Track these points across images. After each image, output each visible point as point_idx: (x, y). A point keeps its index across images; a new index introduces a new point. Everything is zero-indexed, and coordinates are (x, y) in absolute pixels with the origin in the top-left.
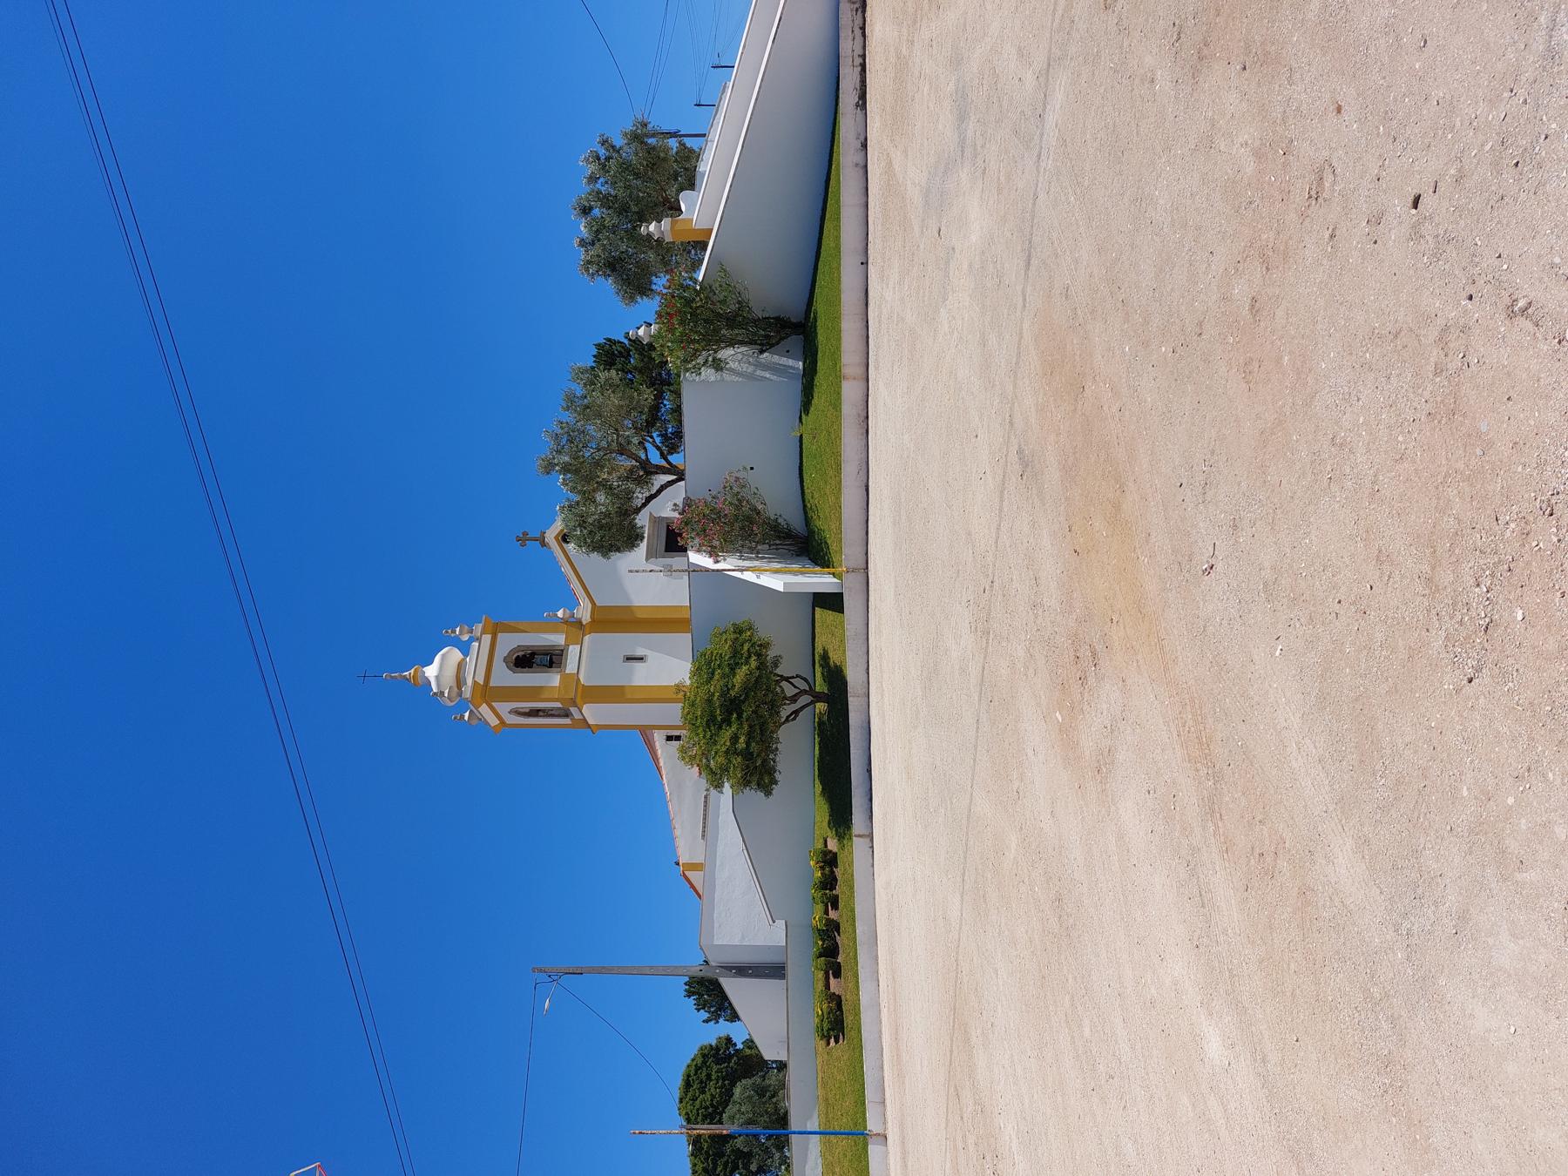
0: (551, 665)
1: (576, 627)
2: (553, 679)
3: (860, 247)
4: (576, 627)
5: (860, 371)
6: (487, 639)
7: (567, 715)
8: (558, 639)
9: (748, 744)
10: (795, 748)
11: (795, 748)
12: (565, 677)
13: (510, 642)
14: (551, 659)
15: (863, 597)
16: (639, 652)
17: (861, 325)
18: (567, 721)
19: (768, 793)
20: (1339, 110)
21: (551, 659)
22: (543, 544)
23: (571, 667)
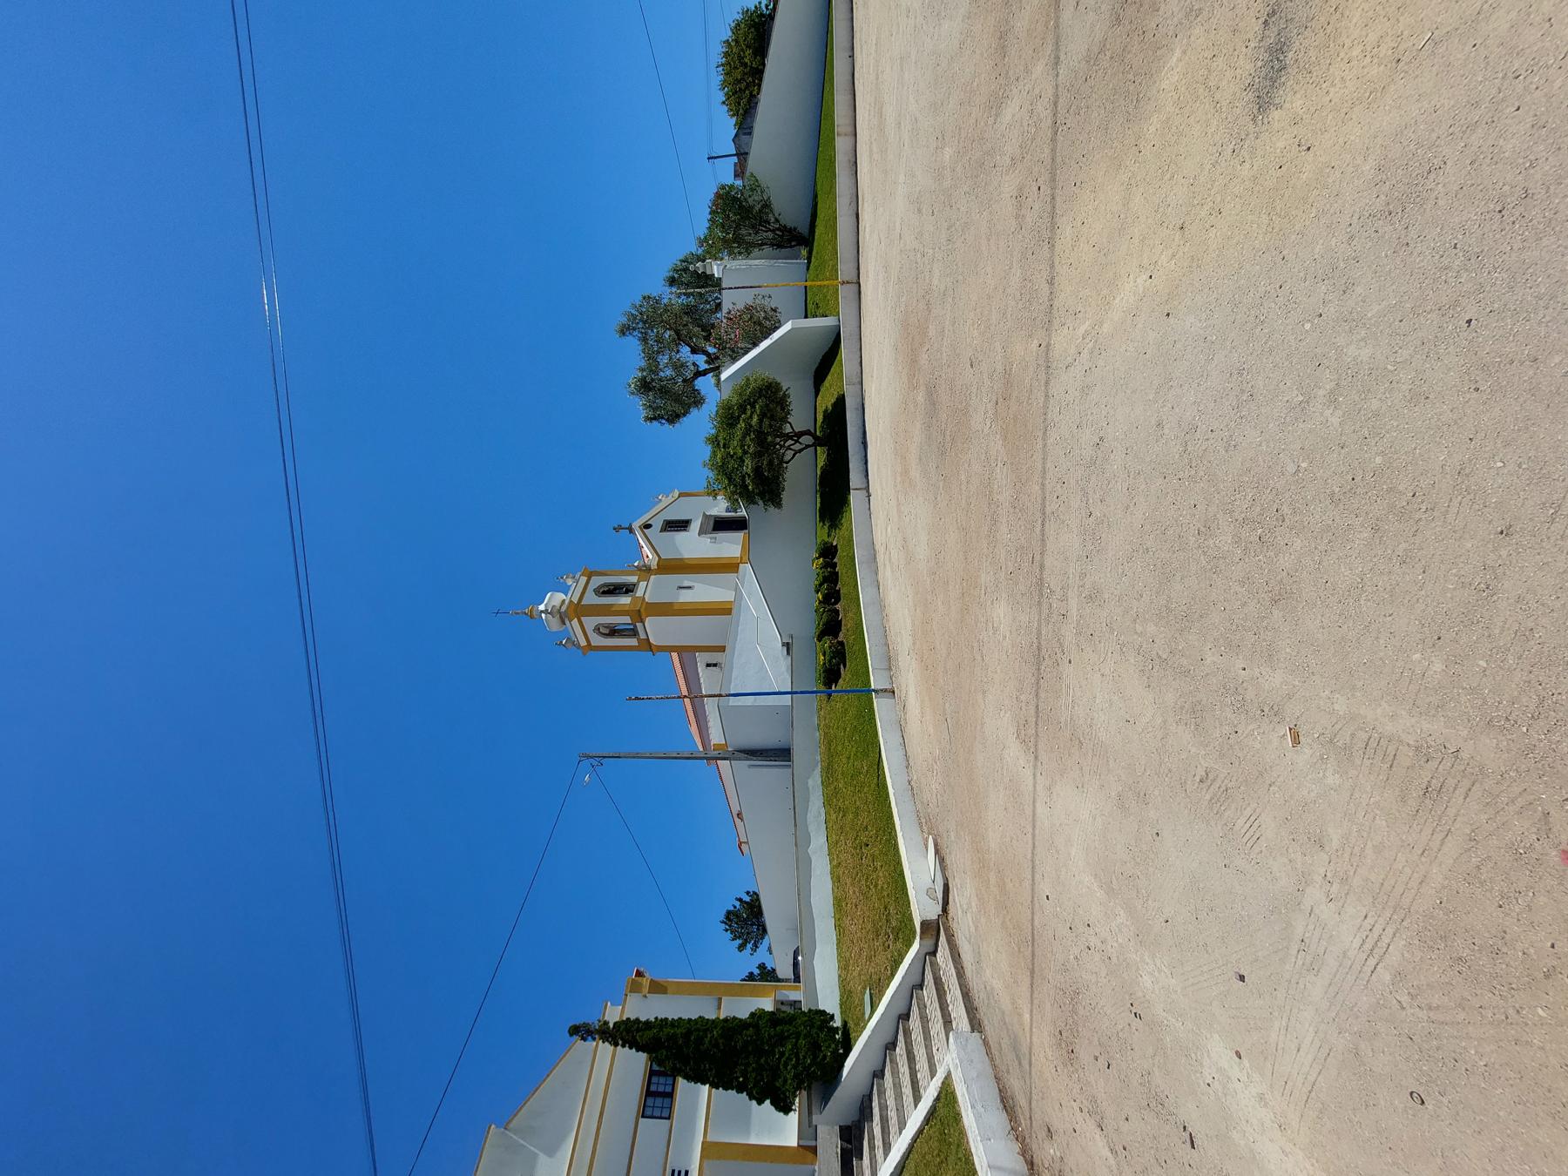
0: (627, 592)
1: (646, 571)
2: (625, 600)
3: (849, 70)
4: (646, 571)
5: (850, 129)
6: (584, 579)
7: (633, 633)
8: (633, 579)
9: (761, 421)
10: (801, 471)
11: (801, 471)
12: (635, 599)
13: (597, 581)
14: (628, 589)
15: (855, 305)
16: (686, 584)
17: (850, 97)
18: (633, 642)
19: (778, 504)
20: (1242, 978)
21: (628, 589)
22: (631, 530)
23: (639, 593)
